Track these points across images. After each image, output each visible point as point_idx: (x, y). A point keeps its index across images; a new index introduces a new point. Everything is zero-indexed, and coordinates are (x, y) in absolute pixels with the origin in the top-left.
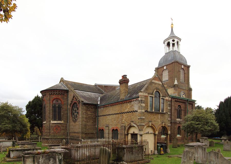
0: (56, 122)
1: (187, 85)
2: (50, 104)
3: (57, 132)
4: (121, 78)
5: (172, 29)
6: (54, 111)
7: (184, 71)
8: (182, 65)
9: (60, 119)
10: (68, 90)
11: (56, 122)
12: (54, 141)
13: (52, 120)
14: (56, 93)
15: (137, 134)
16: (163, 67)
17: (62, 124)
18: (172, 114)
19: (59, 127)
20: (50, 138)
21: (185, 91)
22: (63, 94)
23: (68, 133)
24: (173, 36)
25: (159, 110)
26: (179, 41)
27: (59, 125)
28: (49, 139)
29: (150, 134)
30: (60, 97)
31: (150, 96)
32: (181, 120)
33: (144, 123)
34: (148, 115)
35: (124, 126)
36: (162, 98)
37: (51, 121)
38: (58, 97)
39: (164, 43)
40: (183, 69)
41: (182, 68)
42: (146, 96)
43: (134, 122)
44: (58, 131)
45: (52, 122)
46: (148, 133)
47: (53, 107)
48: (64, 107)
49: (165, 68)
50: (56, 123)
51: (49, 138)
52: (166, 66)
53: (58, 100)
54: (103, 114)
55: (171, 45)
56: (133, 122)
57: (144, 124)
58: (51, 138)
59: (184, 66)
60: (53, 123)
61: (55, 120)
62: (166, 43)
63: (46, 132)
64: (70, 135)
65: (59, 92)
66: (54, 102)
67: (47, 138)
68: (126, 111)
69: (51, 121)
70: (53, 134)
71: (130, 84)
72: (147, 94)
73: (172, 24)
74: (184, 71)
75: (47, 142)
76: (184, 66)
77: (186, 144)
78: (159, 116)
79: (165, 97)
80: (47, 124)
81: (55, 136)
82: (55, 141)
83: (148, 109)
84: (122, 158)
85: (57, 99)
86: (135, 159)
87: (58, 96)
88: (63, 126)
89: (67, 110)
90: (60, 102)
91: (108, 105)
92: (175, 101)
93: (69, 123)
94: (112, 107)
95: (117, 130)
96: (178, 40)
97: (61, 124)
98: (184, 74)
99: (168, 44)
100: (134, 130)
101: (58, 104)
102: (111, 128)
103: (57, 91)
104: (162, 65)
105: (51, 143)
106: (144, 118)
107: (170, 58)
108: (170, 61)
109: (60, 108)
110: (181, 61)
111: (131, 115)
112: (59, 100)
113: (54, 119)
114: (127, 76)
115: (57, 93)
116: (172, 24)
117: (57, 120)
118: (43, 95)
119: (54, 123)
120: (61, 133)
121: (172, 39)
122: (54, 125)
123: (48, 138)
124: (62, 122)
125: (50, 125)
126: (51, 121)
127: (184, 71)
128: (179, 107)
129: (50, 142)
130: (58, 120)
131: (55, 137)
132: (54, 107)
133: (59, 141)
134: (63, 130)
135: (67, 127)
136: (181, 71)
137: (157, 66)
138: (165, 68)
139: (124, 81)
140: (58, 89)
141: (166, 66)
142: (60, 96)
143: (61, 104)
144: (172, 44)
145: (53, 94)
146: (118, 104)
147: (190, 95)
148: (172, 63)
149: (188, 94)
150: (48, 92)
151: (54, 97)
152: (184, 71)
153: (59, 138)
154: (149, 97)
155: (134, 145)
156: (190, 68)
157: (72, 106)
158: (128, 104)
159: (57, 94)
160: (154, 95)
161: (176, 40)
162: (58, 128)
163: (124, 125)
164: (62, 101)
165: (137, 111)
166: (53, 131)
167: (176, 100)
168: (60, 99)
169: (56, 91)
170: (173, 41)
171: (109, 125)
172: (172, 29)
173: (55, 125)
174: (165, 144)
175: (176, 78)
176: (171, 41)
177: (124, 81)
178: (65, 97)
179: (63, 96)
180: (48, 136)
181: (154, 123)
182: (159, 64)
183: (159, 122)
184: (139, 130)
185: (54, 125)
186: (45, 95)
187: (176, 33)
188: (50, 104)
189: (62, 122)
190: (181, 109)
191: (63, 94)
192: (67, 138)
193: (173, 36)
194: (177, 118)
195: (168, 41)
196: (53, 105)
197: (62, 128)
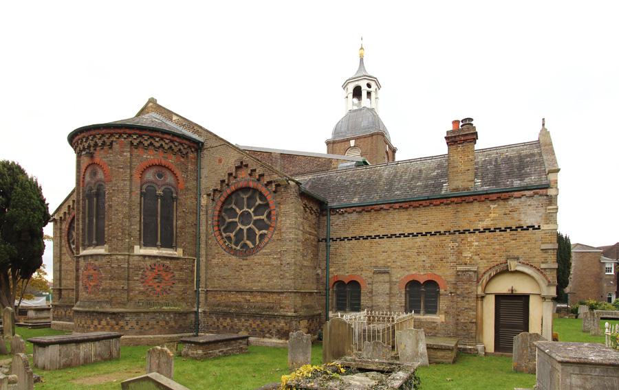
0: (154, 251)
2: (131, 180)
3: (159, 289)
5: (362, 60)
6: (148, 213)
9: (168, 243)
10: (203, 144)
11: (154, 251)
12: (151, 322)
13: (140, 245)
14: (157, 145)
15: (526, 298)
16: (348, 140)
17: (178, 259)
19: (167, 269)
20: (130, 313)
22: (184, 152)
23: (197, 292)
27: (167, 263)
28: (123, 317)
30: (171, 160)
35: (475, 272)
37: (137, 248)
38: (163, 162)
39: (345, 86)
43: (521, 260)
44: (162, 285)
45: (139, 250)
47: (142, 194)
48: (187, 200)
49: (352, 143)
50: (155, 257)
51: (126, 312)
52: (356, 139)
53: (164, 170)
54: (357, 234)
55: (364, 94)
56: (517, 259)
58: (135, 310)
60: (144, 256)
61: (148, 243)
62: (351, 87)
63: (104, 290)
64: (209, 299)
65: (171, 144)
66: (150, 176)
67: (114, 313)
68: (480, 226)
69: (133, 248)
70: (142, 297)
71: (480, 145)
73: (362, 48)
75: (92, 326)
77: (426, 302)
80: (114, 257)
81: (149, 304)
82: (153, 322)
85: (160, 165)
87: (165, 155)
88: (181, 269)
89: (197, 213)
90: (170, 179)
91: (385, 207)
93: (203, 259)
94: (406, 213)
95: (432, 284)
97: (174, 262)
99: (357, 92)
100: (513, 285)
101: (163, 188)
102: (400, 276)
103: (166, 136)
104: (344, 136)
105: (137, 330)
107: (365, 124)
108: (365, 129)
109: (169, 199)
111: (506, 239)
112: (168, 173)
113: (97, 239)
114: (472, 122)
115: (162, 145)
116: (362, 48)
117: (159, 243)
118: (78, 149)
119: (150, 256)
120: (173, 291)
121: (367, 82)
122: (149, 262)
123: (119, 313)
124: (179, 253)
125: (128, 262)
126: (137, 248)
129: (132, 328)
130: (162, 246)
131: (152, 309)
132: (148, 194)
133: (167, 323)
134: (181, 280)
135: (192, 271)
138: (352, 143)
139: (462, 135)
141: (356, 139)
142: (174, 157)
143: (174, 188)
145: (146, 148)
146: (448, 204)
148: (372, 135)
150: (90, 138)
151: (150, 157)
153: (168, 313)
155: (377, 313)
157: (220, 198)
158: (492, 206)
159: (161, 150)
162: (164, 274)
163: (475, 269)
164: (179, 178)
165: (539, 228)
166: (144, 286)
168: (170, 170)
169: (160, 135)
171: (388, 267)
172: (362, 60)
173: (153, 261)
174: (339, 300)
177: (462, 135)
178: (190, 167)
179: (182, 160)
180: (124, 304)
182: (336, 132)
184: (549, 282)
185: (149, 262)
186: (104, 144)
188: (131, 180)
189: (179, 253)
191: (184, 152)
192: (196, 309)
196: (144, 187)
197: (177, 274)
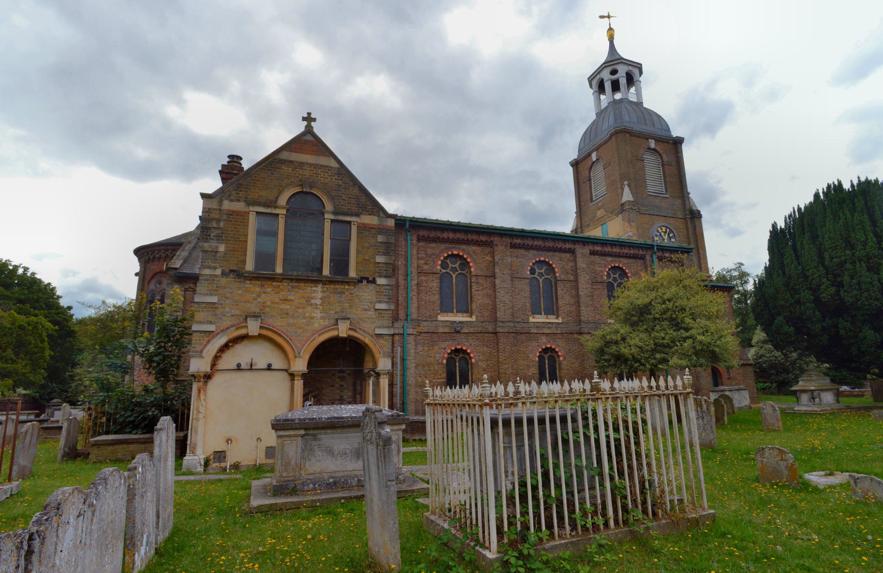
1: (678, 202)
4: (225, 161)
5: (611, 39)
7: (662, 158)
8: (647, 139)
18: (583, 299)
21: (672, 221)
24: (614, 60)
25: (320, 269)
26: (636, 71)
29: (276, 372)
31: (257, 213)
32: (469, 319)
33: (211, 322)
34: (240, 288)
36: (332, 221)
40: (654, 150)
41: (649, 148)
42: (240, 212)
46: (251, 369)
49: (594, 157)
52: (597, 149)
55: (608, 86)
57: (212, 328)
59: (658, 140)
62: (595, 83)
72: (239, 206)
73: (611, 29)
74: (660, 155)
76: (656, 140)
78: (318, 292)
79: (352, 215)
83: (244, 262)
84: (116, 461)
86: (657, 409)
92: (593, 253)
96: (631, 68)
98: (663, 165)
99: (601, 88)
106: (214, 299)
110: (644, 127)
121: (609, 70)
127: (662, 158)
128: (617, 276)
136: (649, 158)
137: (574, 155)
140: (551, 253)
141: (597, 149)
144: (609, 82)
147: (695, 235)
149: (688, 232)
152: (660, 155)
154: (252, 218)
156: (684, 147)
160: (283, 208)
161: (622, 70)
167: (598, 248)
170: (614, 72)
172: (611, 39)
175: (626, 182)
176: (606, 75)
181: (278, 323)
183: (312, 318)
187: (624, 52)
190: (555, 277)
193: (614, 60)
194: (534, 313)
195: (598, 77)
